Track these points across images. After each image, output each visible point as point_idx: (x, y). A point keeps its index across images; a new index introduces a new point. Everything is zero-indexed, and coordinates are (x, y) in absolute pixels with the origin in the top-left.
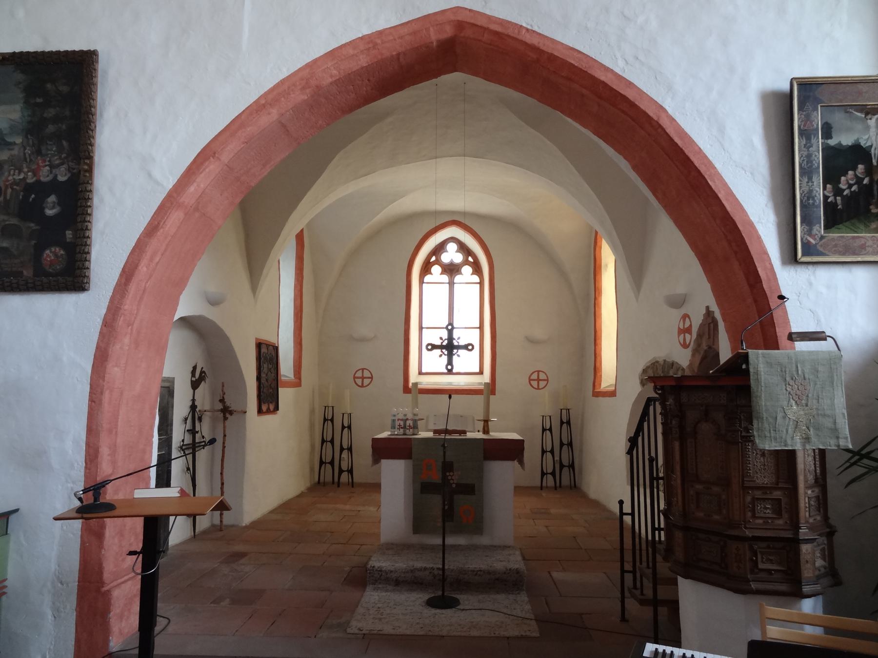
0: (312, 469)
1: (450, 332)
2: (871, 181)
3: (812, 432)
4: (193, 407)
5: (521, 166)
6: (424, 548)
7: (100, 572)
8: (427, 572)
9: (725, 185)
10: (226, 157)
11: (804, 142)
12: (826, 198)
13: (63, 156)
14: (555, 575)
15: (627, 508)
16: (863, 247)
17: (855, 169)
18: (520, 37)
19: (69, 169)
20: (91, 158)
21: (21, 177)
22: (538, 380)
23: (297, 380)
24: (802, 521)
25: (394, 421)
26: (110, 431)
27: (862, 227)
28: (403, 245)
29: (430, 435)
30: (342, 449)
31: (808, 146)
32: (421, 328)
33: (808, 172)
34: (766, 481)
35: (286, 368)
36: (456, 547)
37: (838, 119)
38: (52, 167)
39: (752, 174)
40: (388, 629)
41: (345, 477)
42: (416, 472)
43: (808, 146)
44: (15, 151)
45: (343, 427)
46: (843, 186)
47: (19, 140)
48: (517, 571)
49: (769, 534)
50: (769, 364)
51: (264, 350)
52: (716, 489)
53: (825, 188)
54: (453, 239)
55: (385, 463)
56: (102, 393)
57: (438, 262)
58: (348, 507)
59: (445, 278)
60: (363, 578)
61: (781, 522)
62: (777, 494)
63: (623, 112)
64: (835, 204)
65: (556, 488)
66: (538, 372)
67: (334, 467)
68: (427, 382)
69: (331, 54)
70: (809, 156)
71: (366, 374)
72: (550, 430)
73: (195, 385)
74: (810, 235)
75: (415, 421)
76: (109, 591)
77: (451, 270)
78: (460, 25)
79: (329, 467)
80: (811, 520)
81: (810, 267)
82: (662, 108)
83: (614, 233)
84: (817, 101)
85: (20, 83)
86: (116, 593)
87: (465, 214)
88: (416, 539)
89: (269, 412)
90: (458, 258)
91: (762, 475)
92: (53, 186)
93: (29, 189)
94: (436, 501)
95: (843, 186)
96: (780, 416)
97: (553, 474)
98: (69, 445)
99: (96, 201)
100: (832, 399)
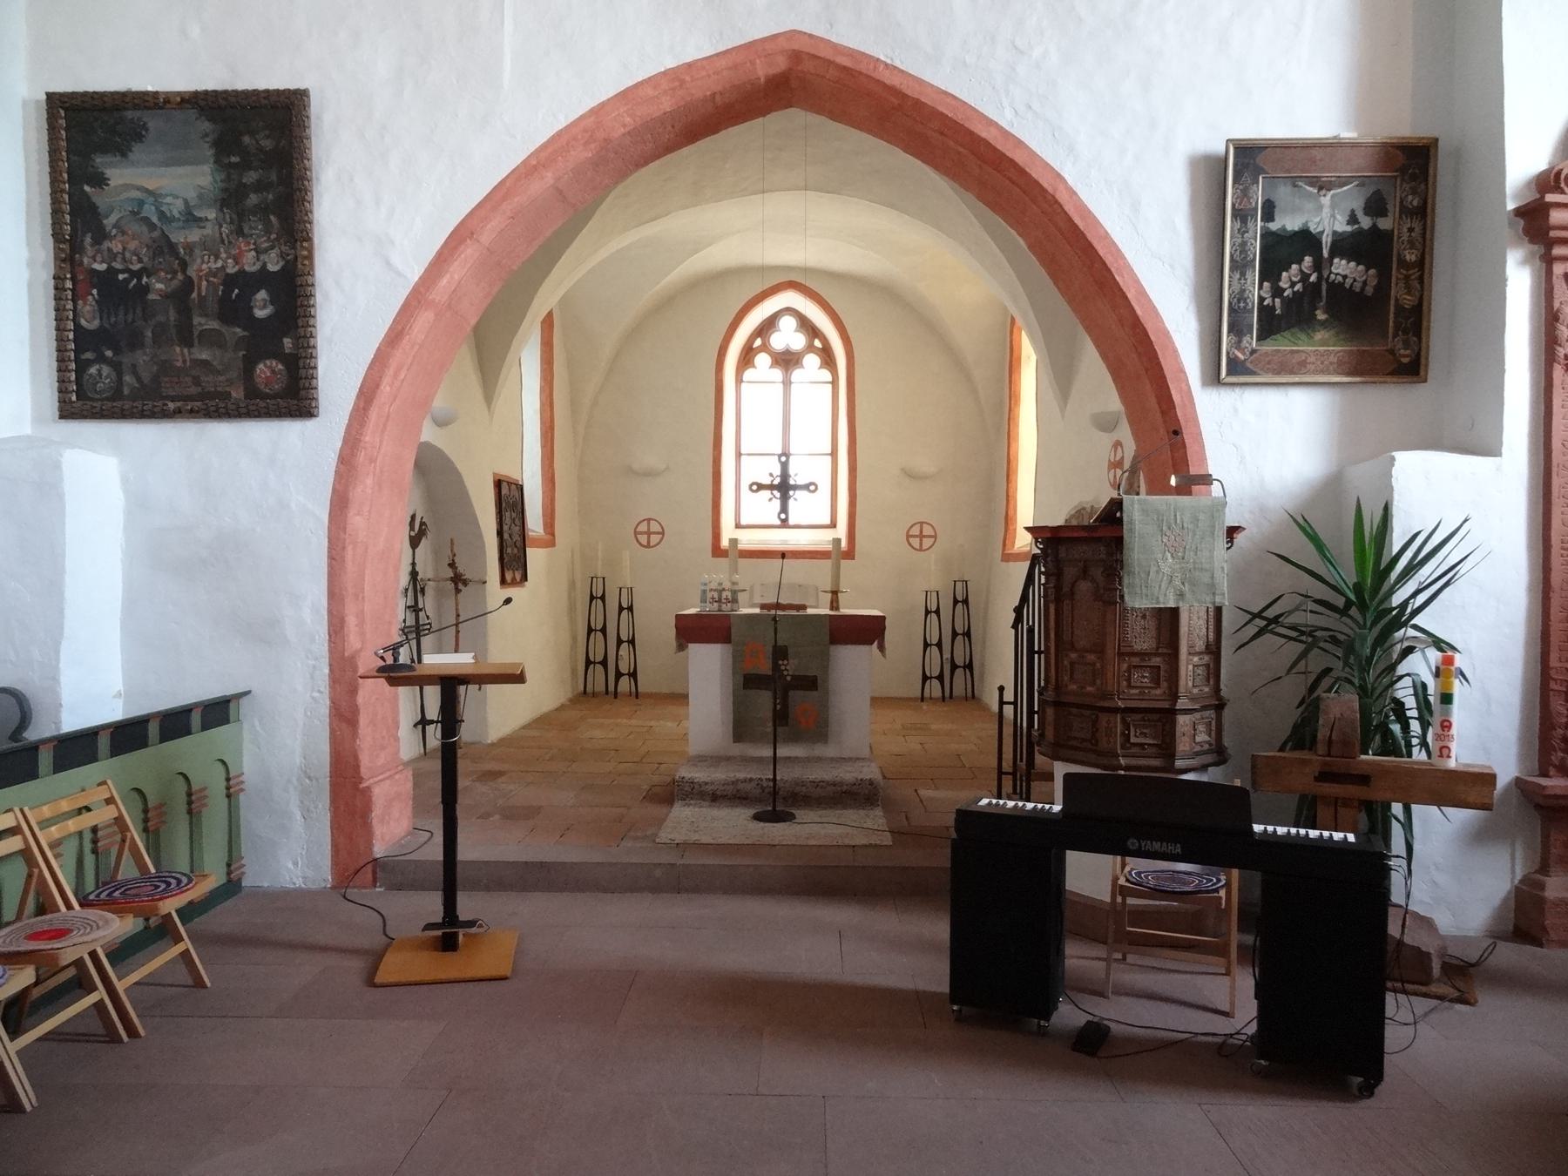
0: (574, 672)
1: (785, 466)
2: (1320, 278)
4: (414, 574)
5: (892, 206)
6: (746, 760)
7: (357, 767)
8: (753, 784)
9: (1137, 281)
10: (487, 237)
12: (1261, 299)
13: (273, 236)
14: (922, 792)
15: (1009, 696)
16: (1303, 364)
17: (1300, 262)
18: (875, 75)
19: (282, 255)
20: (309, 239)
21: (220, 264)
22: (921, 536)
23: (548, 537)
24: (1182, 689)
25: (704, 592)
26: (356, 596)
27: (1303, 337)
28: (713, 317)
29: (757, 611)
30: (620, 642)
32: (739, 455)
33: (1240, 266)
34: (1145, 646)
36: (788, 759)
37: (1283, 194)
38: (258, 251)
39: (1172, 266)
40: (706, 839)
41: (624, 684)
42: (737, 659)
44: (209, 230)
45: (621, 609)
48: (871, 782)
49: (1143, 705)
50: (1145, 512)
51: (505, 491)
52: (1091, 657)
53: (1261, 287)
54: (789, 311)
55: (694, 649)
57: (765, 348)
58: (634, 722)
59: (777, 374)
60: (672, 793)
61: (1158, 692)
63: (1010, 179)
64: (1273, 308)
65: (943, 698)
66: (922, 523)
67: (606, 666)
68: (749, 540)
69: (624, 95)
70: (1244, 244)
71: (655, 527)
72: (937, 612)
73: (415, 542)
75: (734, 593)
76: (368, 788)
78: (796, 56)
79: (599, 668)
80: (1195, 691)
81: (1237, 390)
82: (1059, 176)
83: (1031, 314)
84: (1259, 171)
85: (207, 135)
87: (806, 270)
89: (514, 583)
90: (798, 341)
91: (1142, 639)
92: (262, 278)
93: (230, 281)
94: (764, 701)
96: (1153, 569)
97: (940, 678)
98: (307, 615)
99: (319, 298)
100: (1211, 551)
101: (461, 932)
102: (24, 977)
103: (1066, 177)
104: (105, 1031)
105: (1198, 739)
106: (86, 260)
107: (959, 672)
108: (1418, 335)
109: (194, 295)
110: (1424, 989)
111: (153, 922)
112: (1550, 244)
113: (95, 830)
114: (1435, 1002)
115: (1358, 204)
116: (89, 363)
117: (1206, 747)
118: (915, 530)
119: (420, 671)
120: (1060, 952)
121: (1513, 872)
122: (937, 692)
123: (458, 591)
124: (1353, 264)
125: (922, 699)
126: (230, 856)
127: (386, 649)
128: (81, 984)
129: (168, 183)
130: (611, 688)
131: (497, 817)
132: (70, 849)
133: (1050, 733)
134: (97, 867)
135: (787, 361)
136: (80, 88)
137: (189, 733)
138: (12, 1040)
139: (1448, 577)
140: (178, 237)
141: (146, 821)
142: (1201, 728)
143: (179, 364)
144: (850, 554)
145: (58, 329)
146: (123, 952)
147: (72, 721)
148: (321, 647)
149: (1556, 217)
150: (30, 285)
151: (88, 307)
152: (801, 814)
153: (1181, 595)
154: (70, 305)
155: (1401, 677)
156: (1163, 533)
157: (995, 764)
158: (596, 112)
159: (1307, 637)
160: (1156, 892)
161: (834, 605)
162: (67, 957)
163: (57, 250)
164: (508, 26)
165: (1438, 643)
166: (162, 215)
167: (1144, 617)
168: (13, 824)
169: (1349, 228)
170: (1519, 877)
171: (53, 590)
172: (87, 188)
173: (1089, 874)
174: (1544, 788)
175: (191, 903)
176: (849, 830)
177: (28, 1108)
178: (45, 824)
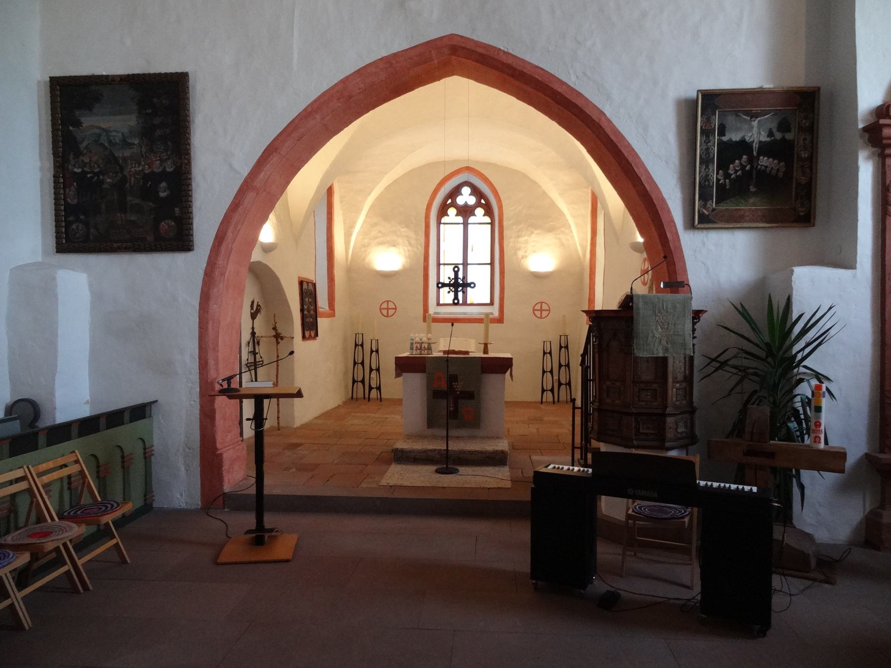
0: (346, 387)
2: (752, 167)
3: (670, 346)
4: (253, 334)
7: (215, 442)
11: (704, 139)
12: (718, 180)
17: (740, 158)
21: (141, 168)
22: (541, 310)
25: (412, 344)
29: (441, 354)
30: (371, 370)
31: (707, 142)
32: (439, 265)
33: (706, 161)
35: (322, 302)
37: (730, 120)
41: (374, 393)
43: (707, 142)
44: (135, 150)
45: (372, 351)
46: (731, 172)
47: (136, 142)
48: (502, 452)
51: (305, 286)
52: (618, 384)
53: (717, 173)
56: (207, 323)
57: (454, 205)
58: (377, 415)
59: (460, 219)
62: (655, 386)
64: (724, 185)
65: (554, 402)
67: (362, 387)
70: (707, 149)
71: (391, 305)
72: (550, 353)
73: (253, 316)
74: (705, 206)
77: (466, 212)
79: (360, 384)
81: (705, 232)
86: (225, 456)
88: (430, 432)
89: (310, 338)
90: (472, 201)
93: (146, 177)
95: (731, 172)
96: (651, 335)
97: (552, 390)
101: (266, 536)
102: (24, 559)
103: (606, 113)
104: (69, 587)
105: (679, 430)
106: (70, 167)
107: (563, 387)
108: (810, 200)
109: (128, 185)
110: (805, 574)
111: (102, 527)
112: (884, 147)
113: (69, 477)
114: (808, 583)
115: (774, 125)
116: (72, 223)
117: (684, 435)
118: (538, 307)
119: (242, 392)
120: (593, 552)
121: (864, 510)
122: (550, 399)
123: (278, 343)
124: (771, 160)
125: (542, 402)
126: (146, 491)
127: (223, 380)
128: (58, 562)
129: (116, 123)
130: (367, 396)
131: (294, 470)
132: (56, 489)
133: (596, 428)
134: (71, 499)
135: (466, 212)
136: (68, 74)
137: (123, 424)
138: (19, 590)
139: (820, 340)
140: (119, 154)
141: (98, 472)
142: (681, 424)
143: (119, 222)
144: (500, 320)
145: (55, 204)
146: (82, 545)
147: (61, 418)
148: (195, 377)
149: (887, 132)
150: (41, 181)
151: (72, 191)
152: (462, 470)
153: (666, 350)
154: (62, 191)
155: (796, 396)
156: (656, 315)
157: (570, 441)
158: (345, 81)
159: (743, 371)
160: (648, 518)
161: (486, 351)
162: (50, 546)
163: (55, 162)
164: (296, 33)
165: (818, 376)
166: (110, 142)
167: (648, 361)
168: (23, 474)
169: (768, 139)
170: (868, 510)
171: (51, 345)
172: (71, 128)
173: (612, 507)
174: (881, 459)
175: (123, 515)
176: (488, 479)
177: (27, 628)
178: (41, 474)
